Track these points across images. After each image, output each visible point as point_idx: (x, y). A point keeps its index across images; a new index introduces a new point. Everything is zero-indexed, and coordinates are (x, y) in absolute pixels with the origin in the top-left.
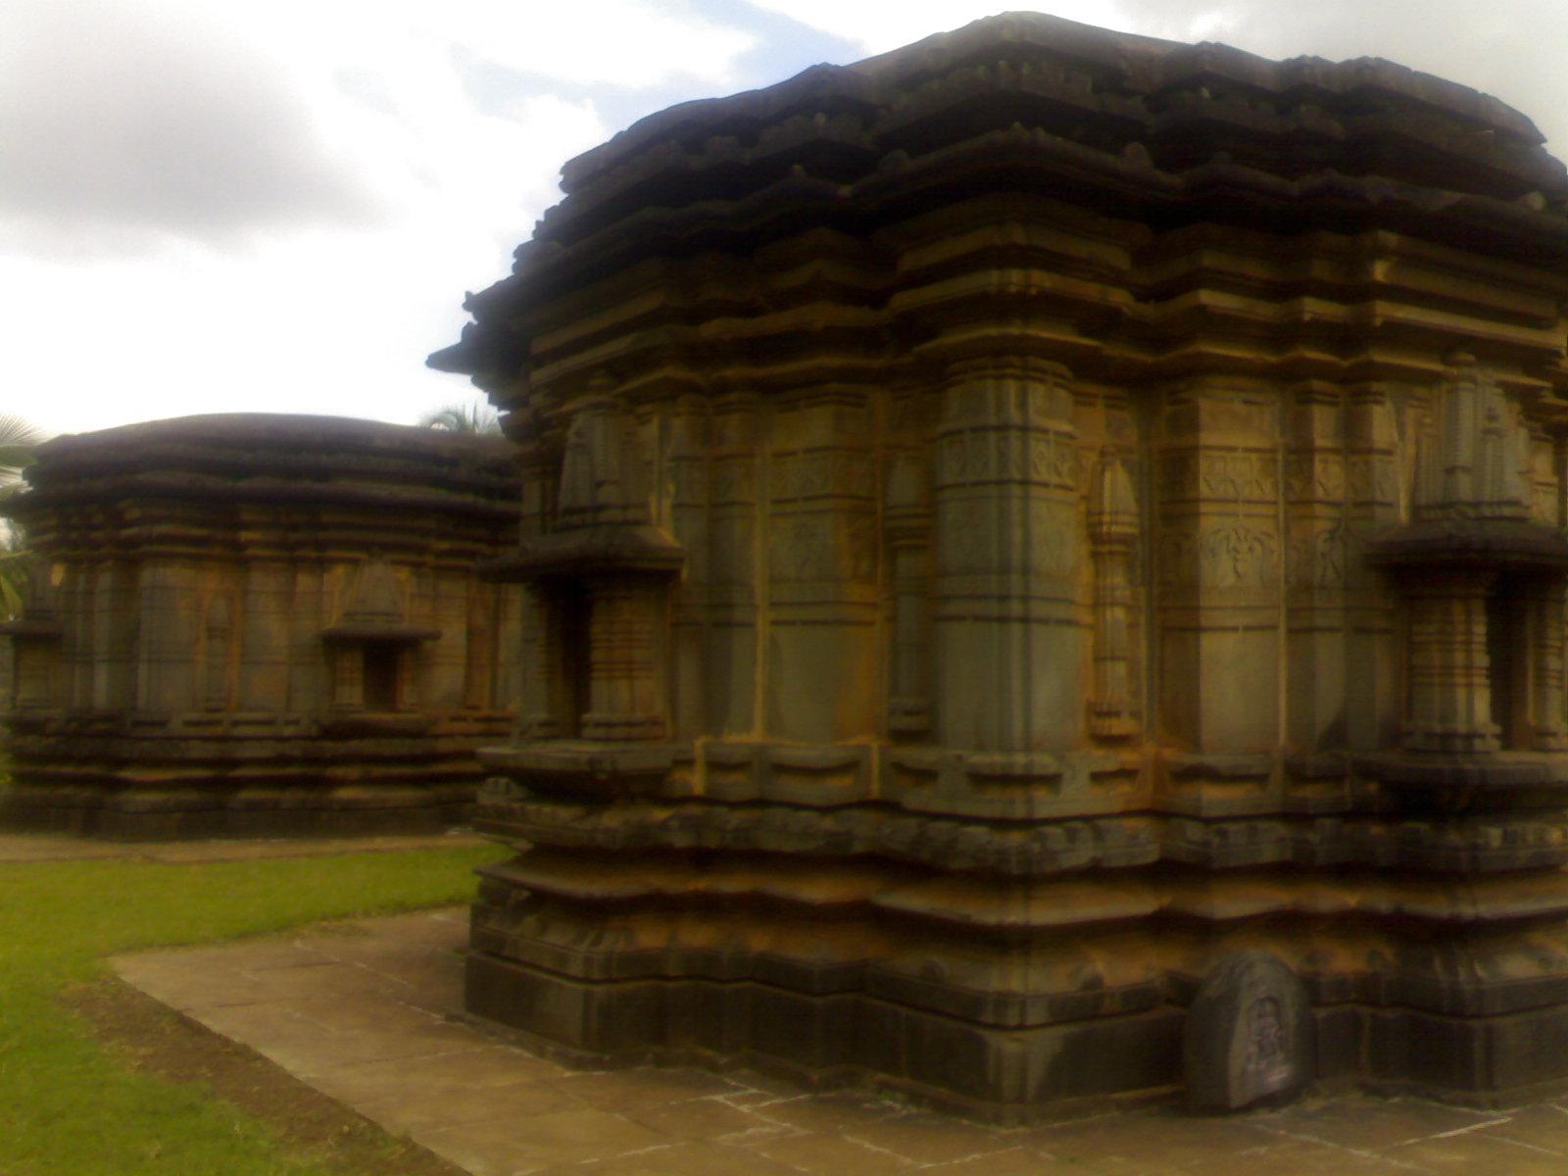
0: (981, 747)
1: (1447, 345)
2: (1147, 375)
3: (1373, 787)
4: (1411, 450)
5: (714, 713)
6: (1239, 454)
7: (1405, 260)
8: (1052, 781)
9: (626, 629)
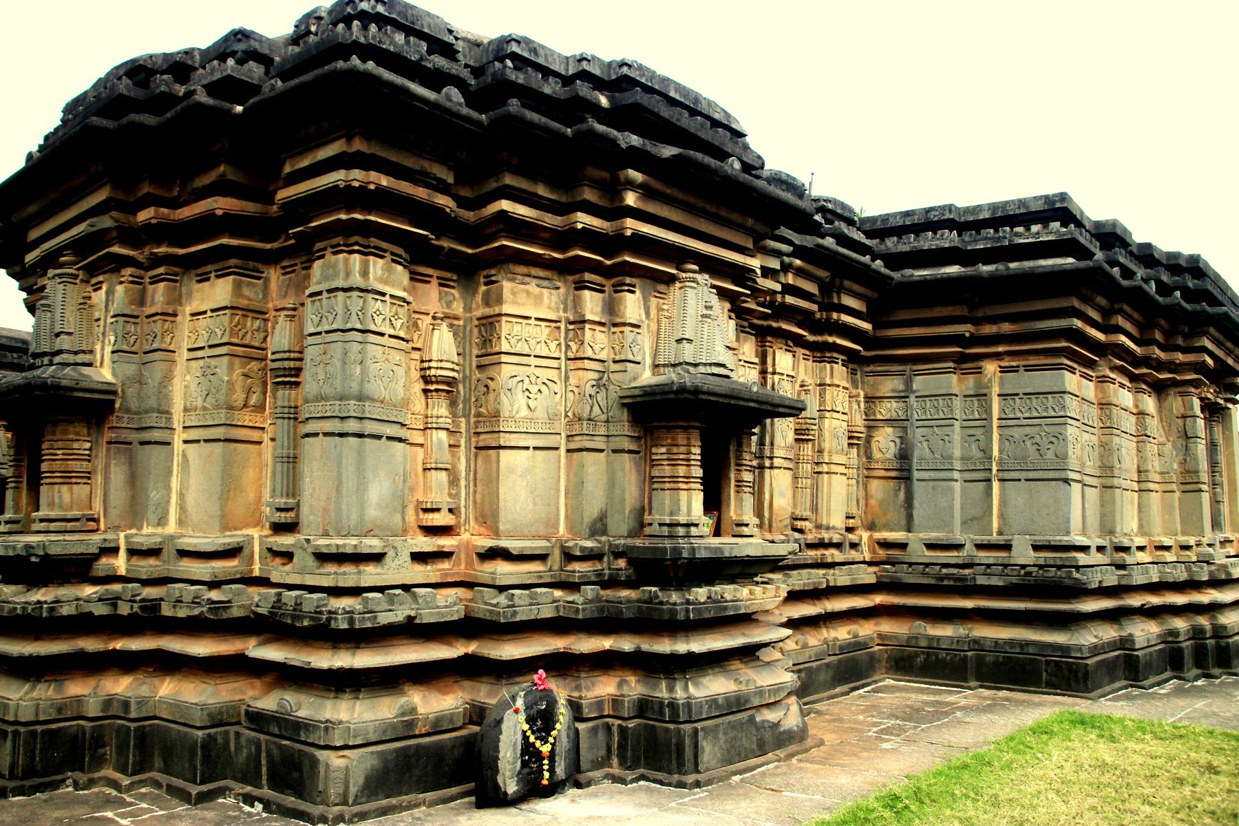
0: (326, 534)
1: (680, 256)
2: (459, 256)
3: (622, 563)
4: (654, 327)
5: (135, 512)
6: (532, 321)
7: (647, 192)
8: (377, 558)
9: (68, 447)
